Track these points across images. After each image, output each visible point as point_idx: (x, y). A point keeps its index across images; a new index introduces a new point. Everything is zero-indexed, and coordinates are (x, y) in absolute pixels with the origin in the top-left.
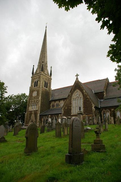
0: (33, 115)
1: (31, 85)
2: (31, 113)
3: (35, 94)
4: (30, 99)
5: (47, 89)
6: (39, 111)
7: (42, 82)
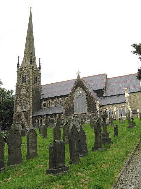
0: (23, 117)
1: (18, 81)
2: (20, 114)
3: (23, 92)
4: (17, 98)
5: (37, 85)
6: (32, 111)
7: (32, 78)
